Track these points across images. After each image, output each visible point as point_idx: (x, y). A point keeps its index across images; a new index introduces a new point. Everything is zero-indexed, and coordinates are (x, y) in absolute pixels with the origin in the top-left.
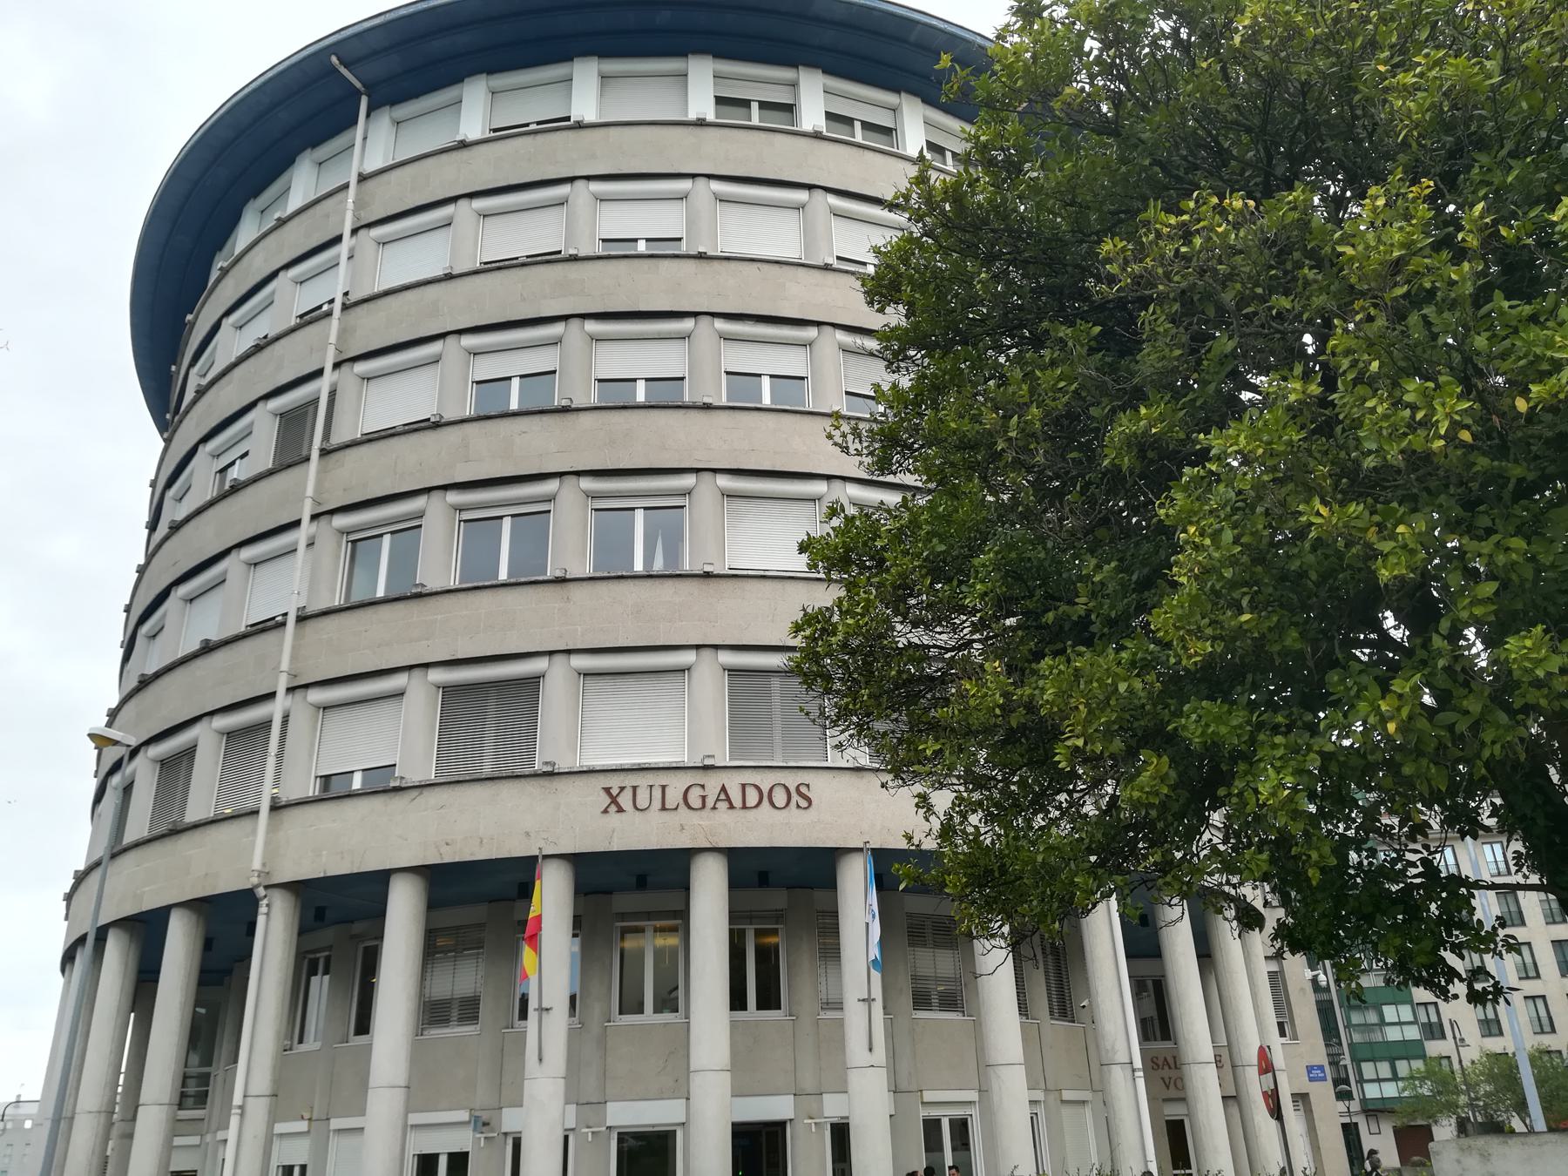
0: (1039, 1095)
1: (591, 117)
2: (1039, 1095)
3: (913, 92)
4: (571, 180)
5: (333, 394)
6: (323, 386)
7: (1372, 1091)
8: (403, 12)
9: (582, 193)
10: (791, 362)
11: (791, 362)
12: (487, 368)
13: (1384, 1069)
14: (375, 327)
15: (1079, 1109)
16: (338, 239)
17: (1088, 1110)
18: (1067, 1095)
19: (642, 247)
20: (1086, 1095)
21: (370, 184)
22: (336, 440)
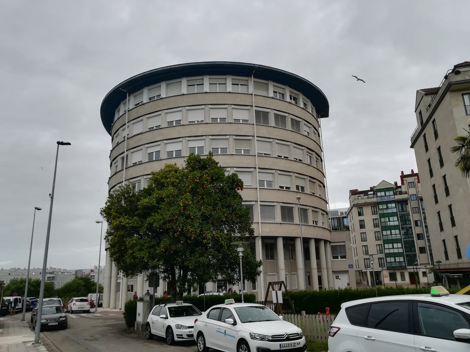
0: (287, 273)
1: (185, 93)
2: (287, 273)
3: (271, 80)
4: (161, 110)
5: (127, 156)
6: (125, 155)
7: (387, 251)
8: (172, 67)
9: (163, 113)
10: (201, 144)
11: (201, 144)
12: (150, 151)
13: (391, 246)
14: (133, 143)
15: (274, 276)
16: (125, 124)
17: (276, 276)
18: (268, 274)
19: (155, 128)
20: (275, 274)
21: (130, 112)
22: (129, 166)
